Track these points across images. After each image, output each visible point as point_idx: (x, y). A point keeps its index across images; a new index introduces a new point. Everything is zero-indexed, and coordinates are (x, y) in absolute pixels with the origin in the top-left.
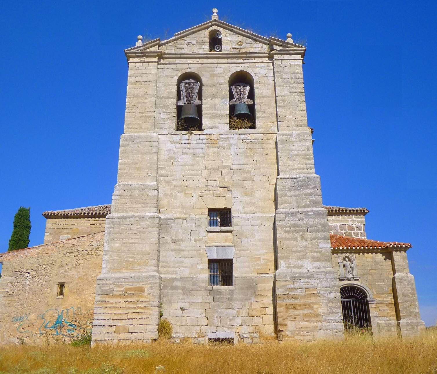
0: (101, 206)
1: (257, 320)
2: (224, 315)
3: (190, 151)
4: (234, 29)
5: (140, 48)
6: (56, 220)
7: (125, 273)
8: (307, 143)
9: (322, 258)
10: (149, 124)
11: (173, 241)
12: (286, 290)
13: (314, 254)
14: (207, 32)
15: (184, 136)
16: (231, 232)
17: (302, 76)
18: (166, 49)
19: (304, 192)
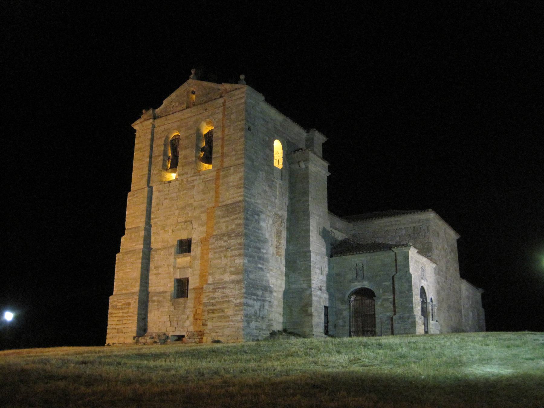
12: (209, 299)
19: (232, 218)
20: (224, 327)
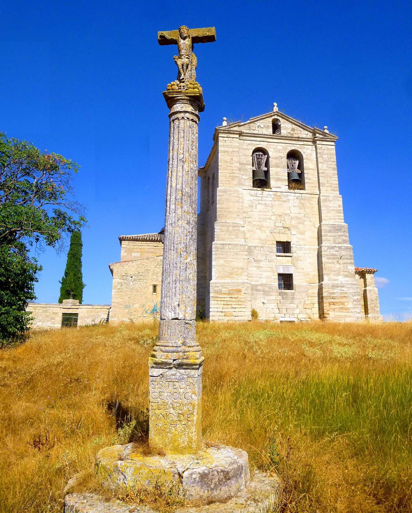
0: (155, 234)
1: (308, 311)
2: (289, 307)
3: (263, 202)
4: (289, 119)
5: (226, 127)
6: (129, 242)
7: (228, 280)
8: (339, 202)
9: (349, 275)
10: (235, 182)
11: (255, 261)
13: (344, 273)
14: (270, 120)
15: (258, 192)
16: (291, 257)
17: (335, 157)
18: (244, 129)
19: (338, 234)
20: (346, 316)
